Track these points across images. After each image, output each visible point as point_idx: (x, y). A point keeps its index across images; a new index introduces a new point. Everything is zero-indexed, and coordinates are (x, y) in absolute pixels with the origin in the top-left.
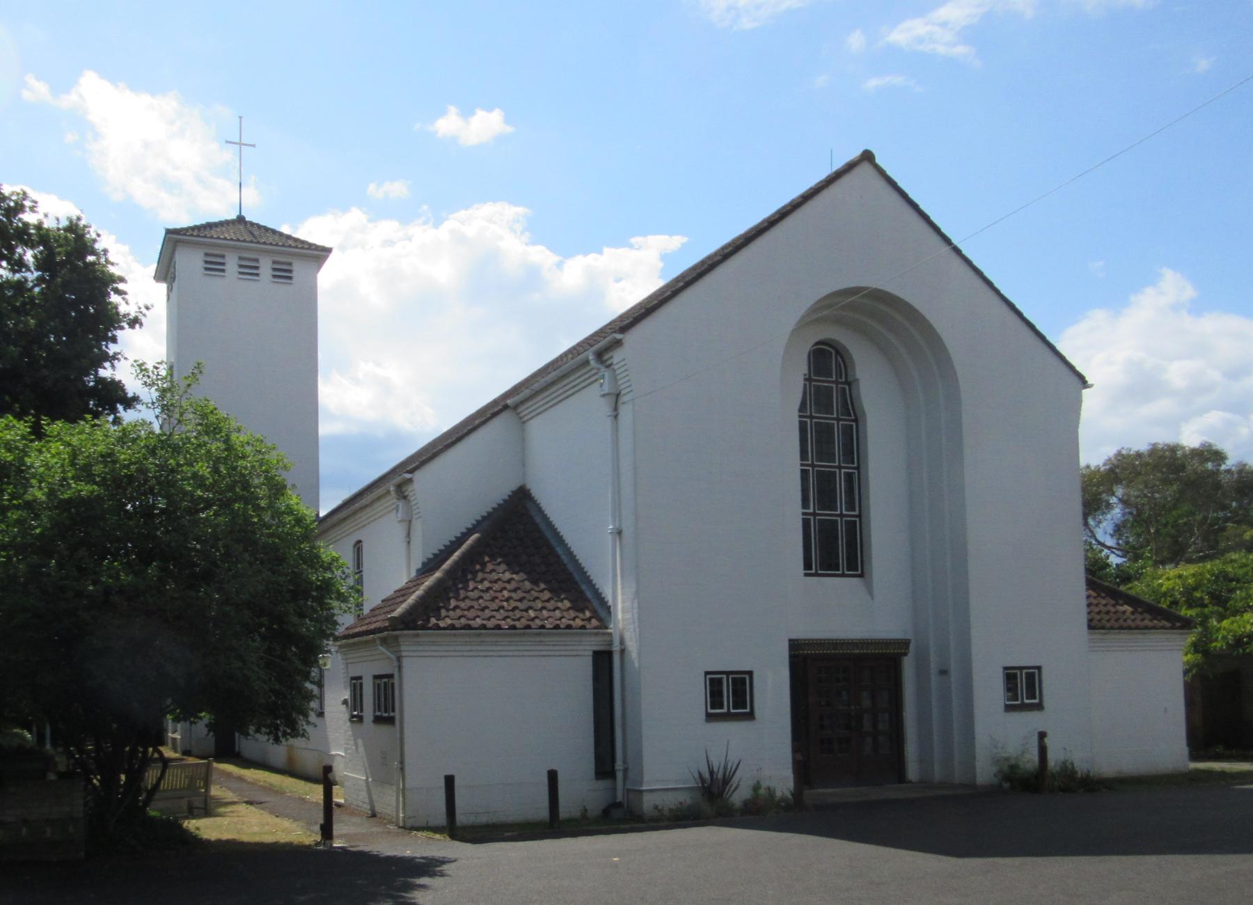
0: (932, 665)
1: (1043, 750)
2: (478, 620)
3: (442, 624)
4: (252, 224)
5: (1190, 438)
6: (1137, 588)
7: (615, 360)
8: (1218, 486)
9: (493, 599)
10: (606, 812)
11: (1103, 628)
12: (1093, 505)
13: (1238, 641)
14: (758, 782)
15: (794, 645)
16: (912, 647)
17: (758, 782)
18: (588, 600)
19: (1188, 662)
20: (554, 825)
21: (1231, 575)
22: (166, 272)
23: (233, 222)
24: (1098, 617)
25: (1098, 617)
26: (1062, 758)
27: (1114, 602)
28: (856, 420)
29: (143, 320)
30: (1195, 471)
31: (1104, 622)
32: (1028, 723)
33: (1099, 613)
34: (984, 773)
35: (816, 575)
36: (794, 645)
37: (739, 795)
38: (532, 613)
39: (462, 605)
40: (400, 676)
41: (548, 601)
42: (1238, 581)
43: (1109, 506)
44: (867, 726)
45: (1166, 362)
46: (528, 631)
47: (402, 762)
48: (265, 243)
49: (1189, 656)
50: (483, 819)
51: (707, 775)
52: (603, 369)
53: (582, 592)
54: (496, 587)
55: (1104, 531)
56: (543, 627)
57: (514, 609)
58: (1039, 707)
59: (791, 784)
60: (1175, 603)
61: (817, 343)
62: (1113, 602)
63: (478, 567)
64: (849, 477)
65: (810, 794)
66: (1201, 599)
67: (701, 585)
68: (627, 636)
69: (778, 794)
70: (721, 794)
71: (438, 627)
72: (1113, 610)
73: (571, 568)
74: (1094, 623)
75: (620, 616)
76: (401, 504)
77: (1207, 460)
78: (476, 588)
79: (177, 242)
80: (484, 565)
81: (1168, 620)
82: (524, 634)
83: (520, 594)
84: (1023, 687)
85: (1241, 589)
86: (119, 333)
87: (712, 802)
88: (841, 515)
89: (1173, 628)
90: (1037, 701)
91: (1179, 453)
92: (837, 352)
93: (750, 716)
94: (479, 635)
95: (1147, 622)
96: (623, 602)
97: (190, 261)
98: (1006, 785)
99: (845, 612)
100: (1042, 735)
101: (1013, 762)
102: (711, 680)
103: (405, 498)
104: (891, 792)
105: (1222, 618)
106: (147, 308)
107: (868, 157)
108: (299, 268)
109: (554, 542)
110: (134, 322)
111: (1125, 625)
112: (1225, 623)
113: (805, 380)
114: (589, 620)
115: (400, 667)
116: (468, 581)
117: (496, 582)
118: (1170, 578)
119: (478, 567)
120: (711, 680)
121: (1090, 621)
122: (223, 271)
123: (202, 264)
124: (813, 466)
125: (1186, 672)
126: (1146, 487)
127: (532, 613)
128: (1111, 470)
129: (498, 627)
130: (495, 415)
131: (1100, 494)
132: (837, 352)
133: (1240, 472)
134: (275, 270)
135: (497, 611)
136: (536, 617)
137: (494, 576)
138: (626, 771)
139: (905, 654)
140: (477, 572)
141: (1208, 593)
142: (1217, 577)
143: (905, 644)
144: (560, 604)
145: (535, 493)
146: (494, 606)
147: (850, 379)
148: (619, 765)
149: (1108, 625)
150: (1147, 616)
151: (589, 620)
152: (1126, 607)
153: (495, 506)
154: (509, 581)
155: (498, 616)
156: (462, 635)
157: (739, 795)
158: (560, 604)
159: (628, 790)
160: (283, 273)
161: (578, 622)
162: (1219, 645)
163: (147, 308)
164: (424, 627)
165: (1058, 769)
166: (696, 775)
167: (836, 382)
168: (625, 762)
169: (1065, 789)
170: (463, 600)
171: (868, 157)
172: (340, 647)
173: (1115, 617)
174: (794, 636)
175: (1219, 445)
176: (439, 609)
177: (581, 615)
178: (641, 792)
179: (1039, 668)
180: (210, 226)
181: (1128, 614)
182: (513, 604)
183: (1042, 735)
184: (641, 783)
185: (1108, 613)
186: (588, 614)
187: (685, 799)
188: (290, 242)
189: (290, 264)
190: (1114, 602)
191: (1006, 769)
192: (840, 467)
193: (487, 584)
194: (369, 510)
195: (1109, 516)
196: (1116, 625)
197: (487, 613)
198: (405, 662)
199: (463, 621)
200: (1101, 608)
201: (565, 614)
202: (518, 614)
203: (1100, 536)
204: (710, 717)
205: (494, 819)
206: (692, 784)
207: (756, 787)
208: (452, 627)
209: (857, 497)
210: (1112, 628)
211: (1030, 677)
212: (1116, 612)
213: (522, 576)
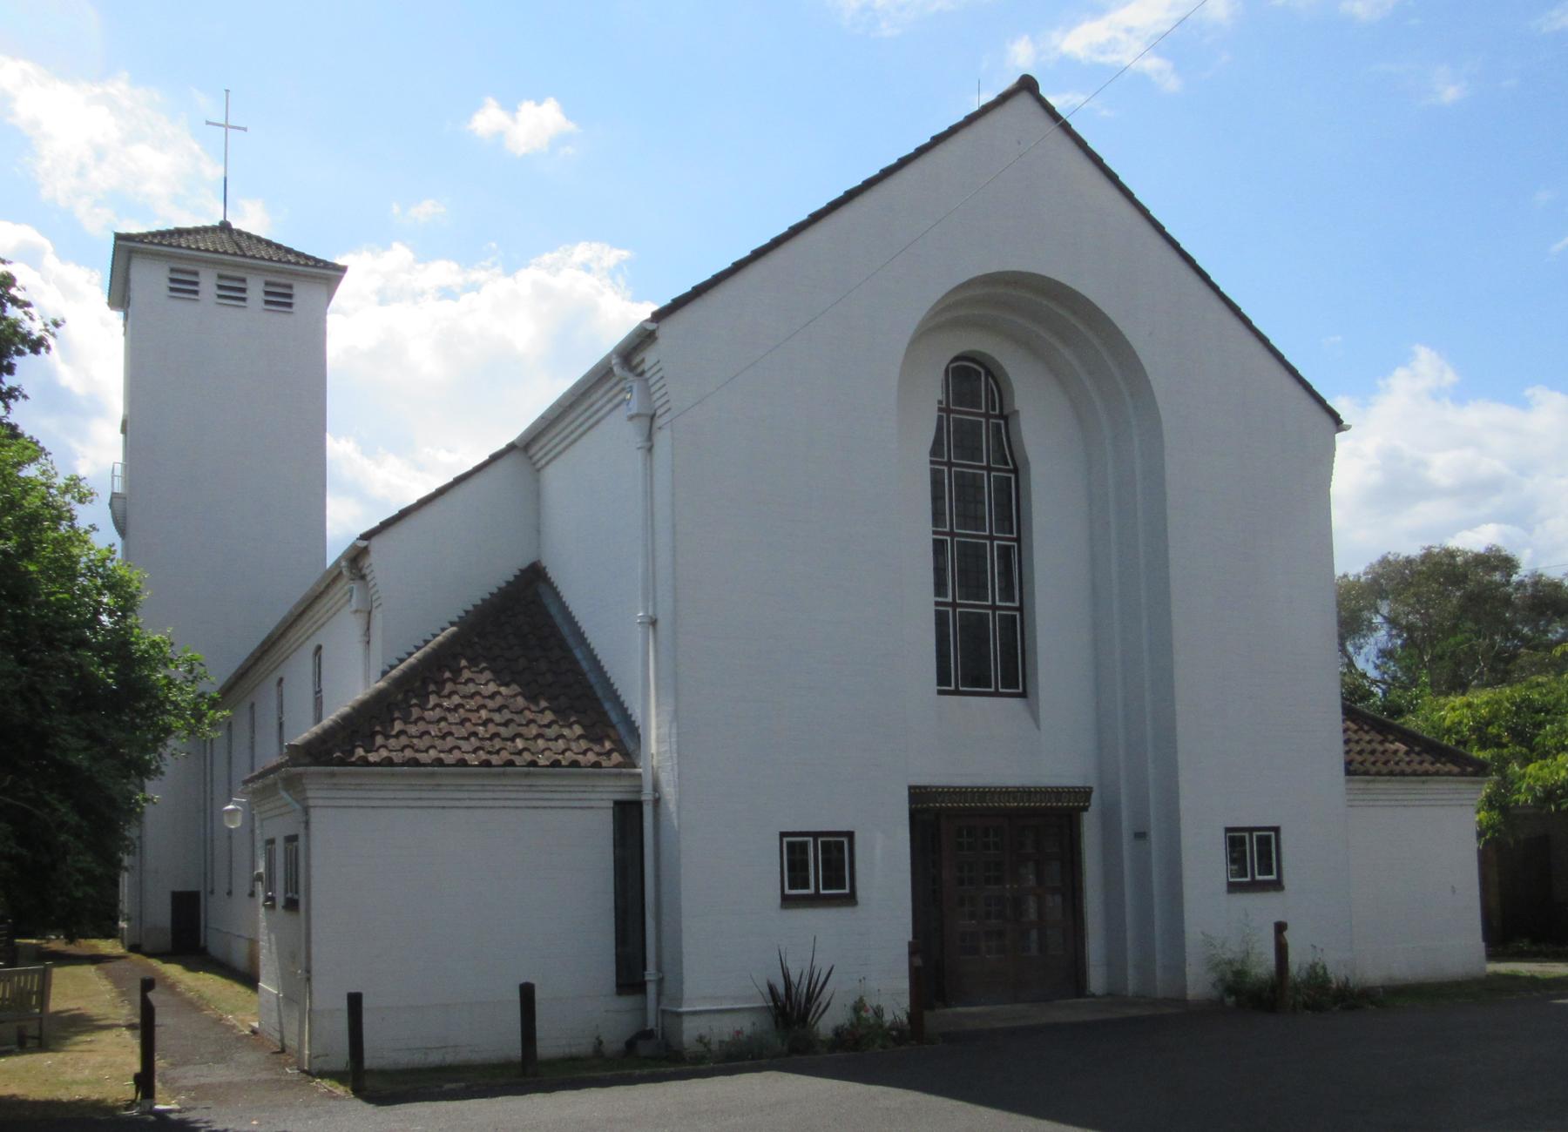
0: (1125, 824)
1: (1281, 949)
2: (432, 753)
3: (372, 757)
4: (240, 233)
5: (1473, 540)
6: (1412, 722)
7: (646, 366)
8: (1507, 601)
9: (462, 722)
10: (630, 1045)
11: (1366, 773)
12: (1351, 625)
13: (1550, 794)
14: (861, 999)
15: (918, 795)
16: (1094, 795)
17: (861, 999)
18: (613, 727)
19: (1480, 822)
20: (529, 1071)
21: (1538, 705)
22: (120, 295)
23: (213, 229)
24: (1359, 758)
25: (1359, 758)
26: (1309, 959)
27: (1381, 739)
28: (1016, 471)
29: (51, 341)
30: (1479, 583)
31: (1367, 764)
32: (1261, 910)
33: (1360, 753)
34: (1198, 982)
35: (956, 692)
36: (918, 795)
37: (832, 1018)
38: (520, 743)
39: (413, 730)
40: (308, 836)
41: (549, 726)
42: (1548, 712)
43: (1372, 629)
44: (1032, 913)
45: (1441, 460)
46: (509, 769)
47: (308, 971)
48: (253, 257)
49: (1483, 814)
50: (435, 1058)
51: (781, 989)
52: (631, 377)
53: (605, 714)
54: (472, 704)
55: (1366, 661)
56: (533, 764)
57: (496, 735)
58: (1277, 885)
59: (905, 1002)
60: (1463, 742)
61: (956, 359)
62: (1380, 738)
63: (447, 675)
64: (1005, 553)
65: (942, 1018)
66: (1499, 736)
67: (791, 707)
68: (665, 777)
69: (888, 1018)
70: (803, 1018)
71: (367, 763)
72: (1380, 748)
73: (592, 678)
74: (1355, 766)
75: (653, 748)
76: (356, 585)
77: (1495, 568)
78: (440, 705)
79: (131, 253)
80: (457, 672)
81: (1454, 763)
82: (504, 774)
83: (507, 715)
84: (1254, 857)
85: (1552, 722)
86: (16, 360)
87: (791, 1033)
88: (994, 607)
89: (1463, 774)
90: (1273, 877)
91: (1459, 560)
92: (989, 373)
93: (850, 899)
94: (432, 775)
95: (1426, 766)
96: (658, 728)
97: (151, 279)
98: (1230, 1000)
99: (991, 747)
100: (1280, 928)
101: (1237, 966)
102: (790, 845)
103: (363, 577)
104: (1065, 1012)
105: (1527, 761)
106: (56, 324)
107: (1027, 85)
108: (303, 294)
109: (571, 641)
110: (37, 345)
111: (1397, 769)
112: (1532, 768)
113: (940, 410)
114: (609, 753)
115: (307, 824)
116: (427, 695)
117: (472, 696)
118: (1453, 711)
119: (447, 675)
120: (790, 845)
121: (1348, 763)
122: (196, 292)
123: (166, 283)
124: (952, 534)
125: (1480, 834)
126: (1418, 601)
127: (520, 743)
128: (1375, 581)
129: (462, 763)
130: (126, 281)
131: (1360, 610)
132: (989, 373)
133: (1536, 584)
134: (267, 293)
135: (467, 739)
136: (525, 749)
137: (471, 688)
138: (660, 982)
139: (1085, 809)
140: (444, 681)
141: (1508, 729)
142: (1519, 708)
143: (1084, 794)
144: (566, 732)
145: (553, 573)
146: (463, 732)
147: (1006, 412)
148: (651, 974)
149: (1374, 769)
150: (1427, 757)
151: (609, 753)
152: (1398, 745)
153: (495, 590)
154: (492, 696)
155: (465, 745)
156: (403, 775)
157: (832, 1018)
158: (566, 732)
159: (664, 1012)
160: (280, 299)
161: (591, 757)
162: (1522, 798)
163: (56, 324)
164: (342, 762)
165: (1304, 975)
166: (766, 990)
167: (987, 416)
168: (659, 968)
169: (1314, 1006)
170: (415, 722)
171: (1027, 85)
172: (254, 792)
173: (1383, 758)
174: (914, 783)
175: (1508, 550)
176: (373, 734)
177: (597, 748)
178: (680, 1015)
179: (1276, 830)
180: (180, 232)
181: (1401, 754)
182: (492, 728)
183: (1280, 928)
184: (679, 1000)
185: (1373, 752)
186: (608, 745)
187: (746, 1025)
188: (292, 258)
189: (290, 287)
190: (1381, 739)
191: (1229, 976)
192: (992, 538)
193: (456, 699)
194: (324, 600)
195: (1372, 640)
196: (1385, 770)
197: (450, 741)
198: (315, 815)
199: (408, 753)
200: (1363, 745)
201: (573, 745)
202: (498, 744)
203: (1360, 664)
204: (787, 901)
205: (450, 1058)
206: (759, 1003)
207: (859, 1007)
208: (389, 762)
209: (1016, 581)
210: (1379, 774)
211: (1264, 843)
212: (1384, 752)
213: (515, 688)
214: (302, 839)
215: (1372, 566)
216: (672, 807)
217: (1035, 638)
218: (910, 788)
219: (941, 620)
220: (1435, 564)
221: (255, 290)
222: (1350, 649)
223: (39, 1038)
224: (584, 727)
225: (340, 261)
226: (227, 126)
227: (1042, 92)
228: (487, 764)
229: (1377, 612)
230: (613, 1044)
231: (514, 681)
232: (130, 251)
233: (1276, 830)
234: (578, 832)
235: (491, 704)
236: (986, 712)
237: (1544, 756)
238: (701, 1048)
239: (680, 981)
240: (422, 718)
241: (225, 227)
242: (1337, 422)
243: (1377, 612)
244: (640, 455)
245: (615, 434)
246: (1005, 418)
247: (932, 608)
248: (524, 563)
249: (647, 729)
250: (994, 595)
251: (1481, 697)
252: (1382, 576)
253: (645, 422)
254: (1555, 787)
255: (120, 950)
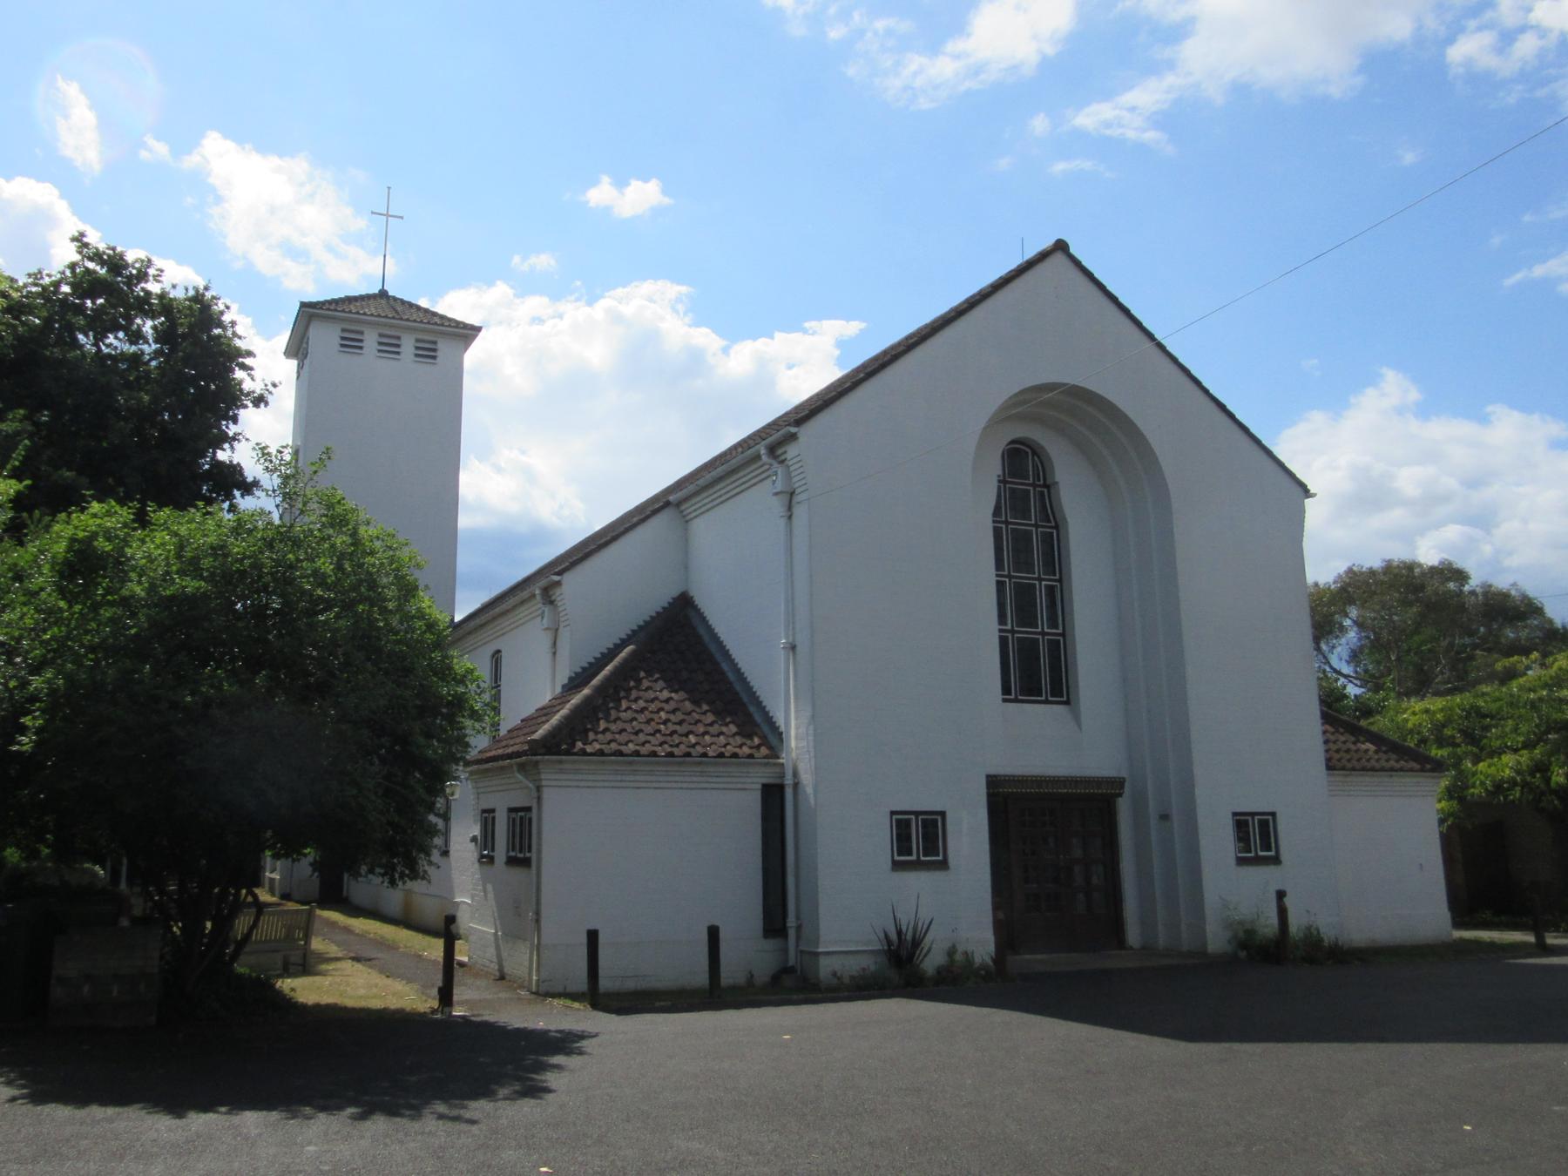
0: (1151, 804)
1: (1282, 912)
4: (395, 299)
5: (1428, 554)
6: (1380, 723)
8: (1462, 608)
9: (649, 721)
11: (1343, 769)
15: (993, 782)
18: (757, 725)
20: (715, 995)
22: (297, 348)
24: (1337, 756)
25: (1337, 756)
27: (1354, 737)
28: (1057, 527)
29: (270, 398)
32: (1261, 880)
33: (1338, 751)
34: (1216, 939)
35: (1016, 701)
36: (993, 782)
37: (931, 962)
38: (692, 739)
39: (613, 727)
41: (711, 724)
42: (1492, 718)
43: (1343, 629)
51: (894, 937)
54: (653, 707)
55: (1339, 658)
56: (705, 755)
58: (1276, 860)
59: (991, 948)
60: (1423, 741)
61: (1012, 442)
64: (1051, 591)
66: (1453, 737)
67: (889, 715)
69: (978, 960)
71: (584, 753)
72: (1353, 747)
73: (738, 687)
74: (1334, 762)
75: (793, 744)
77: (1449, 579)
79: (311, 317)
80: (639, 681)
83: (679, 716)
84: (1256, 836)
85: (1496, 726)
87: (901, 969)
88: (1043, 634)
89: (1422, 770)
90: (1272, 853)
91: (1417, 570)
92: (1034, 453)
93: (943, 865)
94: (630, 763)
95: (1392, 763)
96: (797, 728)
97: (325, 337)
98: (1243, 954)
99: (1045, 744)
100: (1281, 895)
102: (898, 821)
103: (552, 602)
105: (1477, 760)
106: (275, 385)
108: (444, 348)
109: (718, 657)
111: (1369, 765)
114: (758, 747)
115: (539, 799)
117: (652, 701)
118: (1416, 713)
120: (898, 821)
121: (1328, 760)
124: (1009, 576)
125: (1441, 821)
127: (692, 739)
128: (1343, 589)
130: (655, 512)
133: (1486, 594)
137: (651, 694)
138: (799, 928)
139: (1120, 795)
141: (1460, 731)
142: (1469, 713)
143: (1118, 783)
144: (724, 729)
146: (649, 729)
148: (791, 921)
151: (758, 747)
152: (1369, 746)
154: (667, 701)
156: (612, 762)
157: (931, 962)
161: (746, 750)
163: (275, 385)
164: (568, 753)
166: (882, 935)
167: (1034, 485)
168: (798, 918)
172: (471, 773)
173: (1356, 756)
174: (993, 771)
175: (1459, 563)
176: (586, 731)
178: (817, 954)
179: (1273, 814)
180: (350, 300)
182: (671, 727)
183: (1281, 895)
184: (817, 943)
186: (756, 741)
187: (868, 963)
191: (1241, 934)
192: (1040, 580)
193: (641, 703)
195: (1343, 641)
198: (546, 793)
199: (614, 746)
200: (1340, 745)
202: (676, 739)
204: (897, 866)
207: (951, 952)
208: (601, 753)
210: (1353, 769)
211: (1264, 825)
214: (535, 811)
215: (1340, 576)
216: (809, 790)
217: (1074, 654)
218: (988, 776)
219: (1003, 642)
220: (1396, 575)
221: (408, 345)
222: (1324, 647)
223: (303, 965)
224: (738, 726)
225: (455, 305)
226: (388, 215)
227: (1072, 251)
228: (671, 755)
229: (1346, 615)
230: (762, 977)
231: (681, 689)
232: (311, 313)
233: (1273, 814)
234: (731, 808)
235: (667, 707)
236: (1039, 716)
237: (1491, 754)
238: (835, 981)
239: (817, 929)
240: (618, 719)
241: (383, 294)
242: (1307, 493)
243: (1346, 615)
244: (783, 522)
245: (757, 503)
246: (1047, 487)
247: (997, 634)
248: (675, 593)
249: (788, 732)
250: (1043, 623)
251: (1436, 704)
252: (1349, 584)
253: (786, 498)
254: (1502, 781)
255: (274, 899)
